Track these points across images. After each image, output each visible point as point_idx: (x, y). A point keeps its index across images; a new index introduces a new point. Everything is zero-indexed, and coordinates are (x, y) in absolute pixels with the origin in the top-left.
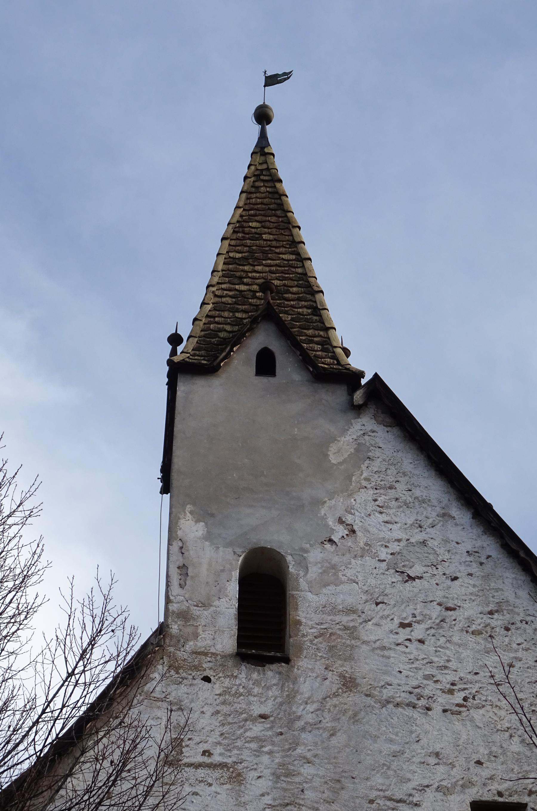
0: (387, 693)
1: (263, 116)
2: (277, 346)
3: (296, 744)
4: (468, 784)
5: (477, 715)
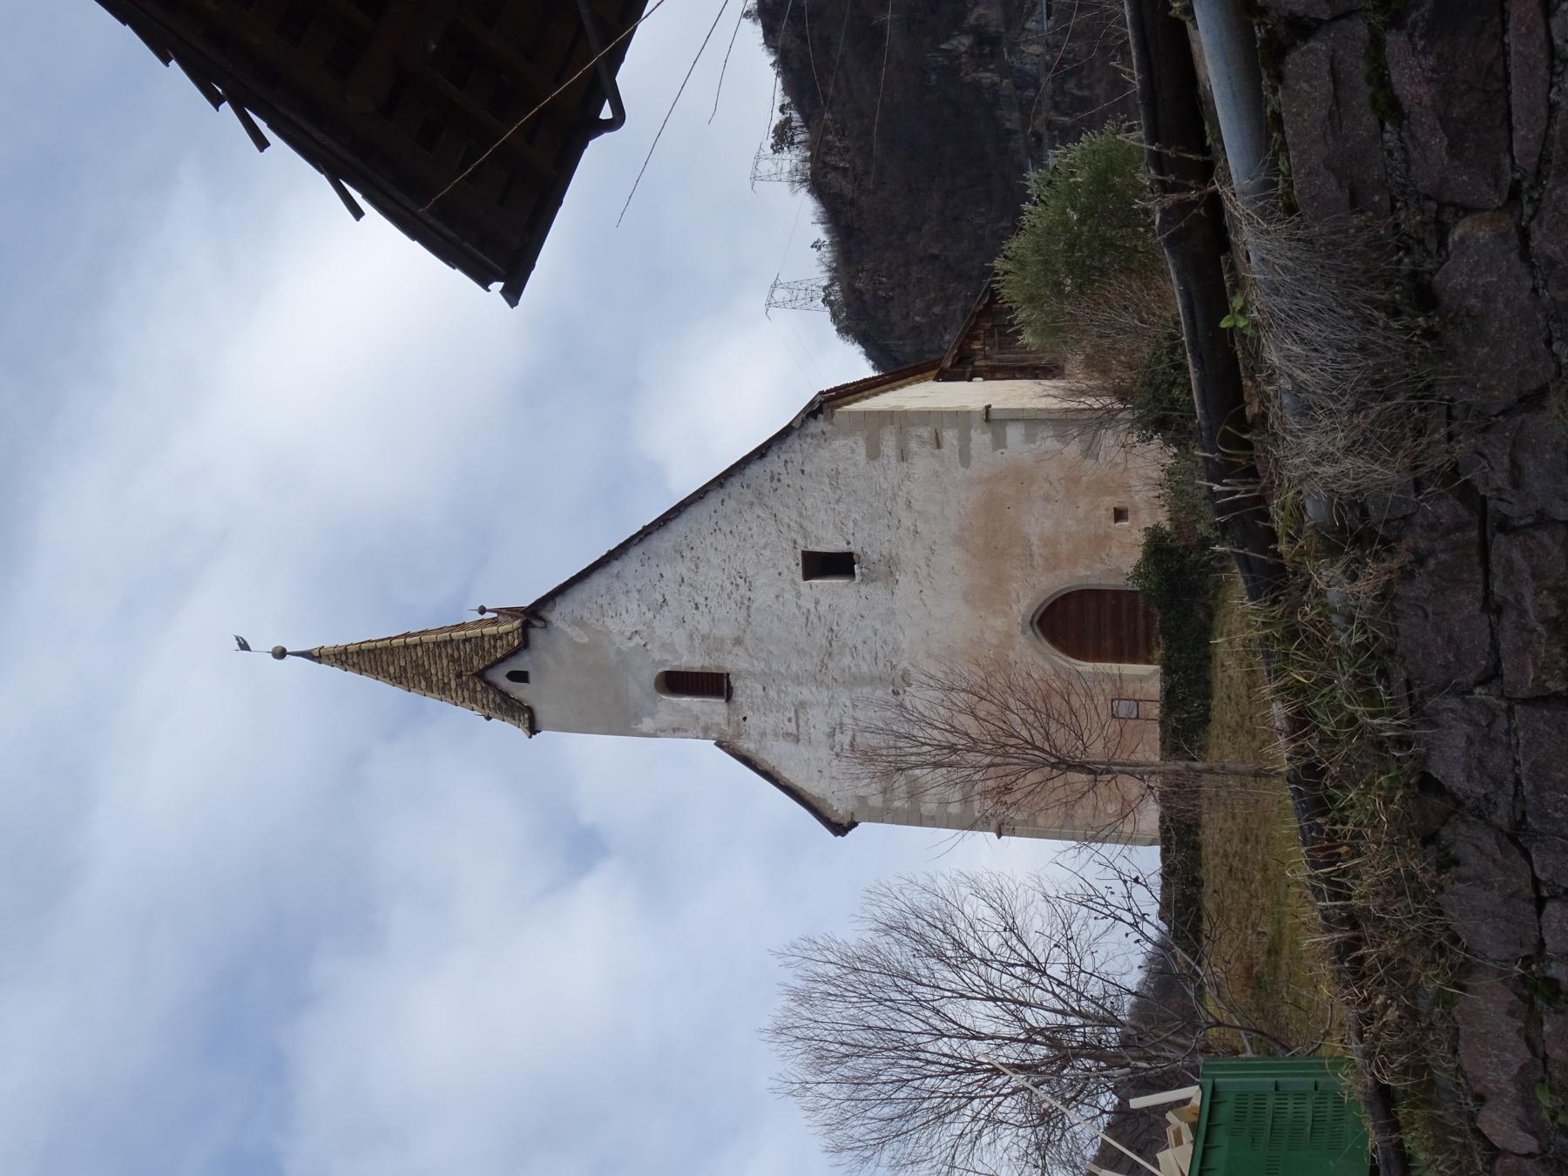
0: (741, 620)
1: (281, 654)
2: (505, 669)
3: (779, 673)
4: (793, 581)
5: (750, 572)
